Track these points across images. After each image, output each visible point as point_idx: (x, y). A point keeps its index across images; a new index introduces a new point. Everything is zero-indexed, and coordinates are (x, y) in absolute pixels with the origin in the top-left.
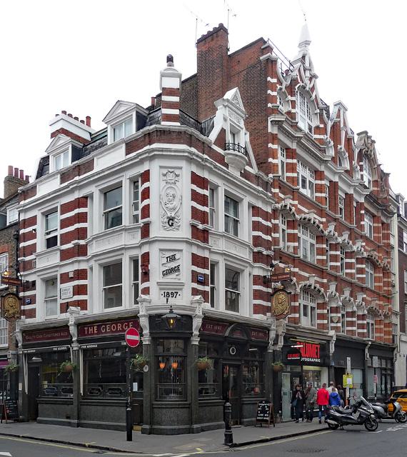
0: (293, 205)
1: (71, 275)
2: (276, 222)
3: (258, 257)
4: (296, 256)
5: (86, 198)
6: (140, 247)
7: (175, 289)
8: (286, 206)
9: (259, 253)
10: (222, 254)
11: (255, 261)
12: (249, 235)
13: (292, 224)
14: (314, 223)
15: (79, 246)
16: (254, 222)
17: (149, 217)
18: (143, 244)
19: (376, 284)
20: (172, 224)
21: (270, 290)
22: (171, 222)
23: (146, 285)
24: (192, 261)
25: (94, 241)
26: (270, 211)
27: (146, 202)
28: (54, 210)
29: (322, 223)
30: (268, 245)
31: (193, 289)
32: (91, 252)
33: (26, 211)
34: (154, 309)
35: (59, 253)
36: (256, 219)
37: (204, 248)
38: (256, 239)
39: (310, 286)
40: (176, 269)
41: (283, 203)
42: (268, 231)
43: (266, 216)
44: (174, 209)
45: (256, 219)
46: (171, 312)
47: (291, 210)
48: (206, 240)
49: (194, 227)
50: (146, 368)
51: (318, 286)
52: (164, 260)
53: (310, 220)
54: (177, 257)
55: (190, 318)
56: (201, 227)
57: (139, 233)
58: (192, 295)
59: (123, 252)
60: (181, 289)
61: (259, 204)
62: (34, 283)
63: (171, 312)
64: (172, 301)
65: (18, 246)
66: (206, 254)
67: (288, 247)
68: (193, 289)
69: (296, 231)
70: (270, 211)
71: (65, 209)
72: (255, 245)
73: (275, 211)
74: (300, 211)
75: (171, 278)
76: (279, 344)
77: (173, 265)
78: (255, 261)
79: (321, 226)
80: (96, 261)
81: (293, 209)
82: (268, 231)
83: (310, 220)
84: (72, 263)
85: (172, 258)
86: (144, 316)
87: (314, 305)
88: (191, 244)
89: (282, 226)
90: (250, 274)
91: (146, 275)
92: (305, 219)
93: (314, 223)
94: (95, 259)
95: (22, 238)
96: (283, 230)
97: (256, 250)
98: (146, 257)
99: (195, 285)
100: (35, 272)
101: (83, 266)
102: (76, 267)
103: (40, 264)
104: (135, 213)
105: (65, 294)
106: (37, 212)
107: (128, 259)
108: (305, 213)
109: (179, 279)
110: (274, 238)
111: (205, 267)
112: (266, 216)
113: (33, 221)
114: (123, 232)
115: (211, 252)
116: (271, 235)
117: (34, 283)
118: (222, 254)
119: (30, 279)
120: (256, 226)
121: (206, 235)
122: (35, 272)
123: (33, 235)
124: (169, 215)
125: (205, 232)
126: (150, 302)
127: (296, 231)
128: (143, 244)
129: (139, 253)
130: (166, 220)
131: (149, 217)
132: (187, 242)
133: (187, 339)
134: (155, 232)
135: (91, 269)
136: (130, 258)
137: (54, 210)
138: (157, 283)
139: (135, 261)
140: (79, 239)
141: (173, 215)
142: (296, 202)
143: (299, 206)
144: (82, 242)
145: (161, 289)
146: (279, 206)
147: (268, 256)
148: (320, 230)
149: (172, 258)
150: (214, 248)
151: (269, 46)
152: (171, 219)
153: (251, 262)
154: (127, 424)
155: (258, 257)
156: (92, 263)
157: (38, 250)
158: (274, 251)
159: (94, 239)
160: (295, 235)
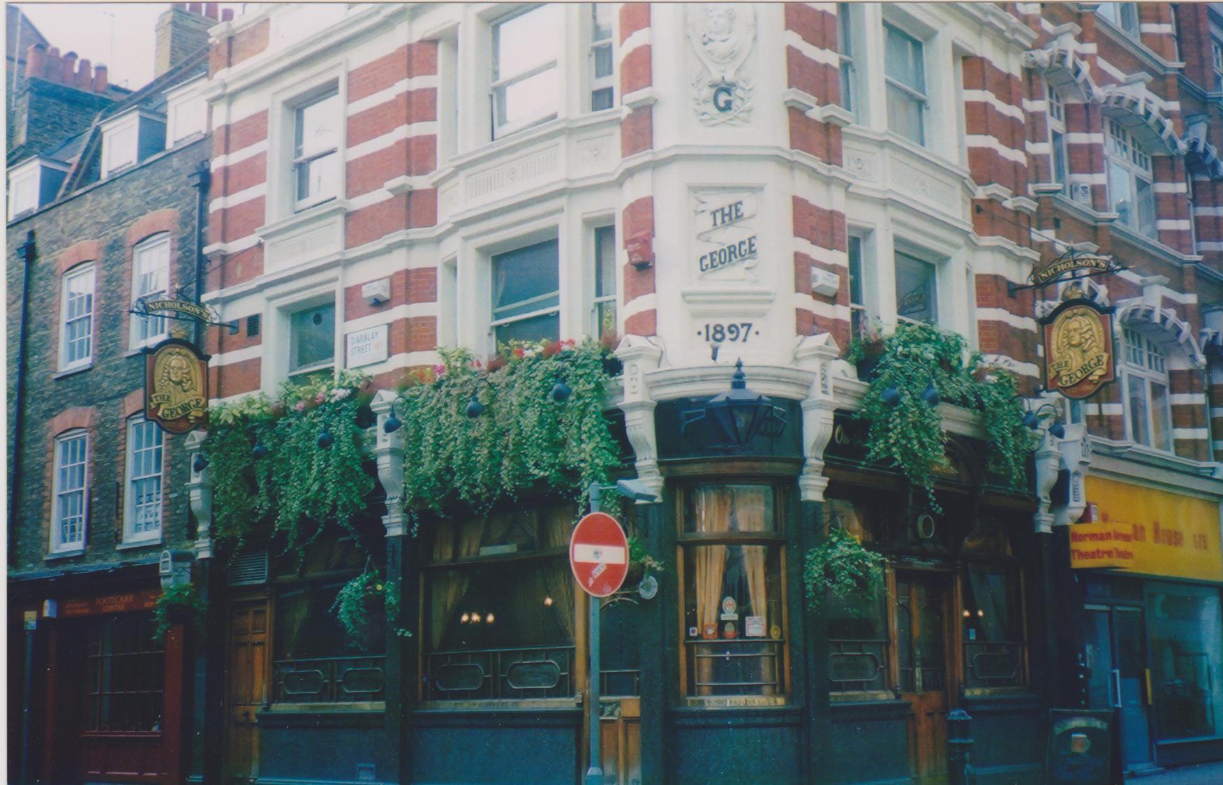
0: (1083, 57)
1: (380, 289)
2: (1040, 106)
3: (986, 215)
4: (1103, 215)
5: (433, 42)
6: (619, 183)
7: (746, 314)
8: (1063, 57)
9: (992, 201)
10: (886, 203)
11: (980, 229)
12: (960, 146)
13: (1082, 116)
14: (1148, 114)
15: (410, 195)
16: (971, 107)
17: (650, 84)
18: (630, 173)
19: (1166, 225)
20: (728, 106)
21: (1029, 324)
22: (723, 98)
23: (642, 304)
24: (796, 219)
25: (462, 174)
26: (1016, 72)
27: (638, 38)
28: (329, 89)
29: (1168, 115)
30: (1016, 177)
31: (801, 314)
32: (448, 212)
33: (231, 98)
34: (674, 382)
35: (340, 219)
36: (978, 96)
37: (828, 181)
38: (978, 157)
39: (1150, 312)
40: (742, 252)
41: (1054, 47)
42: (1013, 133)
43: (1005, 87)
44: (732, 55)
45: (978, 96)
46: (739, 382)
47: (1077, 72)
48: (832, 156)
49: (796, 113)
50: (648, 588)
51: (1172, 314)
52: (706, 222)
53: (1134, 104)
54: (745, 210)
55: (794, 408)
56: (817, 113)
57: (615, 139)
58: (799, 331)
59: (561, 202)
60: (762, 315)
61: (984, 48)
62: (254, 324)
63: (739, 382)
64: (730, 352)
65: (203, 209)
66: (833, 200)
67: (1073, 189)
68: (801, 314)
69: (1096, 138)
70: (1016, 72)
71: (362, 82)
72: (981, 181)
73: (1031, 72)
74: (1103, 78)
75: (731, 278)
76: (1072, 503)
77: (732, 235)
78: (980, 229)
79: (1169, 124)
80: (466, 238)
81: (1085, 67)
82: (1013, 133)
83: (1134, 104)
84: (389, 249)
85: (731, 215)
86: (641, 406)
87: (1163, 379)
88: (791, 165)
89: (1055, 124)
90: (968, 272)
91: (643, 267)
92: (1120, 99)
93: (1148, 114)
94: (465, 231)
95: (217, 184)
96: (1056, 136)
97: (981, 193)
98: (642, 212)
99: (807, 302)
100: (261, 288)
101: (418, 259)
102: (399, 262)
103: (275, 264)
104: (603, 83)
105: (361, 350)
106: (267, 101)
107: (578, 228)
108: (1120, 84)
109: (756, 282)
110: (1033, 158)
111: (831, 243)
112: (1005, 87)
113: (255, 128)
114: (562, 140)
115: (850, 195)
116: (1023, 149)
117: (254, 324)
118: (886, 203)
119: (239, 311)
120: (978, 118)
121: (833, 140)
122: (261, 288)
123: (253, 172)
124: (717, 77)
125: (830, 128)
126: (659, 361)
127: (1096, 138)
128: (630, 173)
129: (616, 204)
130: (708, 93)
131: (650, 84)
132: (777, 159)
133: (786, 486)
134: (666, 136)
135: (452, 267)
136: (587, 223)
137: (329, 89)
138: (684, 295)
139: (603, 233)
140: (409, 173)
141: (729, 77)
142: (1091, 48)
143: (1103, 64)
144: (420, 183)
145: (696, 316)
146: (1043, 56)
147: (1017, 212)
148: (1165, 136)
149: (731, 215)
150: (862, 185)
151: (156, 334)
152: (725, 88)
153: (969, 228)
154: (1178, 29)
155: (986, 215)
156: (453, 246)
157: (274, 215)
158: (1037, 200)
159: (460, 168)
160: (1092, 149)
